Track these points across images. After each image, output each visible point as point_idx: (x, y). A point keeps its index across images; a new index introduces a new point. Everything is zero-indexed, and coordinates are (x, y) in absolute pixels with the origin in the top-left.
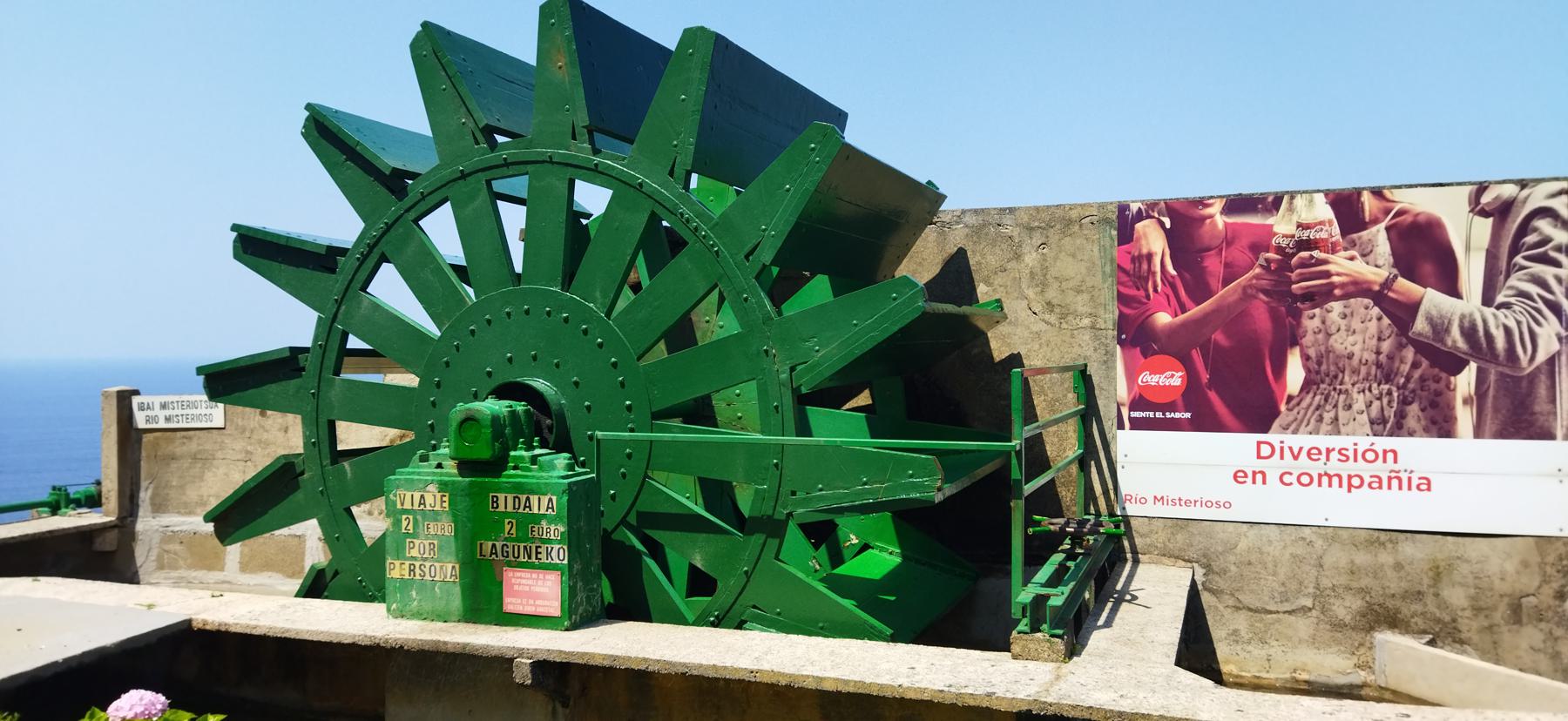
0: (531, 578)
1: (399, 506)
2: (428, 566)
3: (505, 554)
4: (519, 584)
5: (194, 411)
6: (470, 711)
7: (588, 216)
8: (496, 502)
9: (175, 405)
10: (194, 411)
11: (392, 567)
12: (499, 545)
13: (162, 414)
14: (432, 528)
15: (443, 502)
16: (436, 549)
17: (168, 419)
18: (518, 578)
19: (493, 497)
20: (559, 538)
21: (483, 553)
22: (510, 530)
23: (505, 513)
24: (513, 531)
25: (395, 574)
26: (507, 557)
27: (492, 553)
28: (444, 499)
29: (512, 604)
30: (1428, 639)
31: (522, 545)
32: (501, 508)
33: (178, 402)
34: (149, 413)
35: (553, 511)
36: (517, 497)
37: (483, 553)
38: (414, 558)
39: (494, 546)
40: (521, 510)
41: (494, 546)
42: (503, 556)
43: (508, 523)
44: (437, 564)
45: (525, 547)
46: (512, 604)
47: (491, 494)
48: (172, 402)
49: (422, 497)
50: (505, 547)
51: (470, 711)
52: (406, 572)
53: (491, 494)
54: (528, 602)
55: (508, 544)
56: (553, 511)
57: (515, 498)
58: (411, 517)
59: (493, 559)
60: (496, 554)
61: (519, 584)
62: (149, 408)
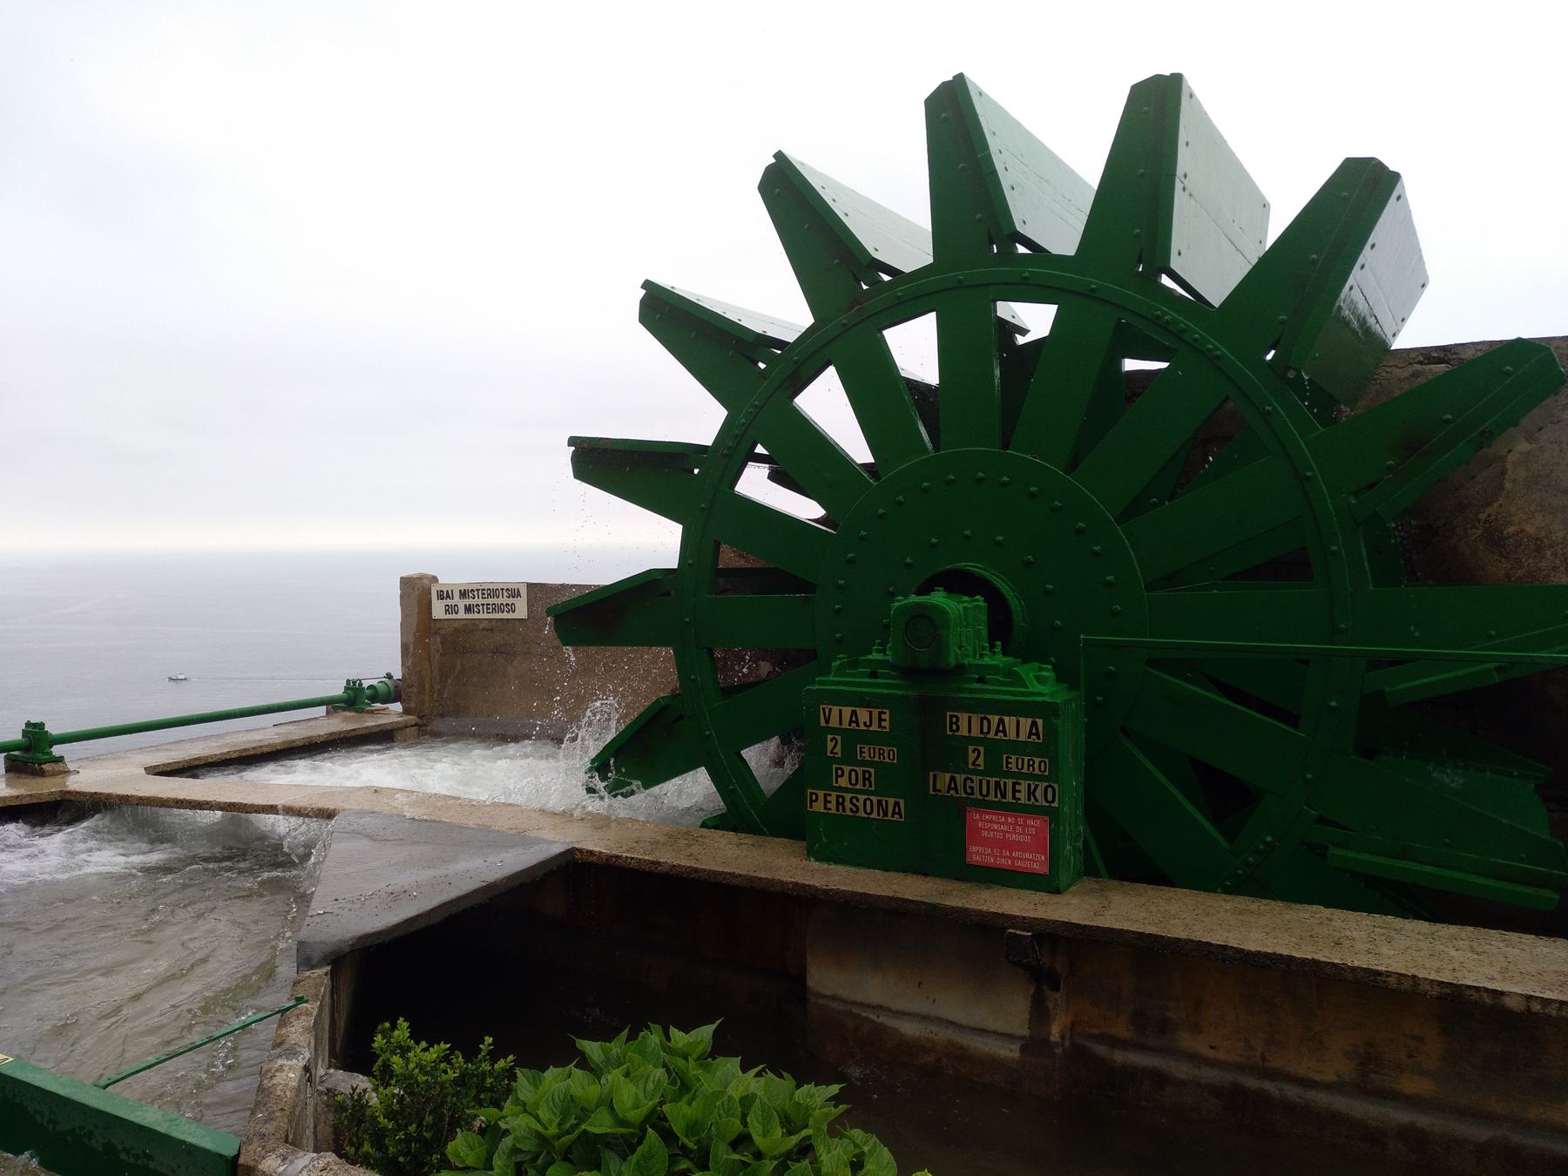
0: (1006, 823)
1: (823, 723)
2: (862, 801)
3: (969, 791)
4: (989, 830)
5: (495, 601)
6: (920, 983)
7: (1024, 332)
8: (956, 723)
9: (476, 593)
10: (495, 601)
11: (814, 798)
12: (960, 778)
13: (462, 604)
14: (867, 752)
15: (881, 720)
16: (872, 779)
17: (468, 609)
18: (987, 821)
19: (951, 716)
20: (1047, 773)
21: (938, 788)
22: (834, 748)
23: (969, 740)
24: (981, 761)
25: (819, 807)
26: (972, 793)
27: (949, 788)
28: (883, 716)
29: (978, 854)
30: (754, 1074)
31: (993, 780)
32: (964, 732)
33: (478, 590)
34: (449, 602)
35: (1038, 738)
36: (985, 718)
37: (938, 788)
38: (841, 789)
39: (953, 779)
40: (991, 735)
41: (953, 779)
42: (966, 792)
43: (973, 752)
44: (874, 799)
45: (997, 784)
46: (978, 854)
47: (948, 713)
48: (472, 590)
49: (854, 712)
50: (969, 782)
51: (920, 983)
52: (833, 806)
53: (948, 713)
54: (1001, 853)
55: (974, 777)
56: (1038, 738)
57: (982, 719)
58: (839, 738)
59: (952, 796)
60: (956, 789)
61: (989, 830)
62: (448, 596)
